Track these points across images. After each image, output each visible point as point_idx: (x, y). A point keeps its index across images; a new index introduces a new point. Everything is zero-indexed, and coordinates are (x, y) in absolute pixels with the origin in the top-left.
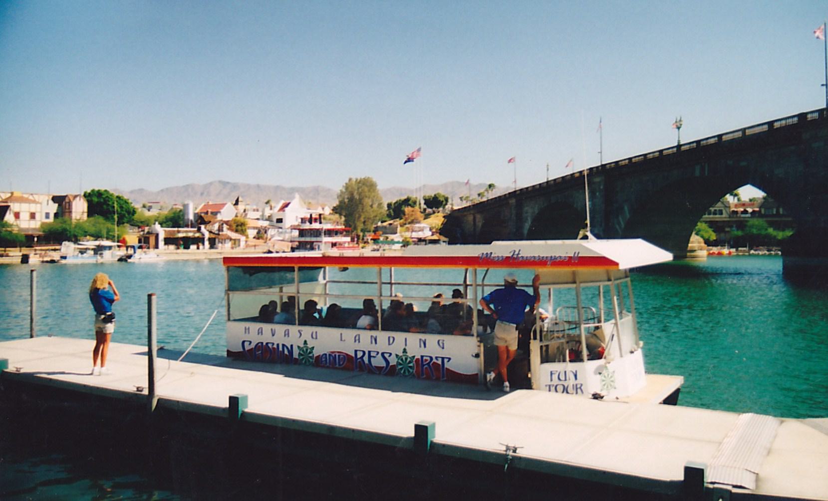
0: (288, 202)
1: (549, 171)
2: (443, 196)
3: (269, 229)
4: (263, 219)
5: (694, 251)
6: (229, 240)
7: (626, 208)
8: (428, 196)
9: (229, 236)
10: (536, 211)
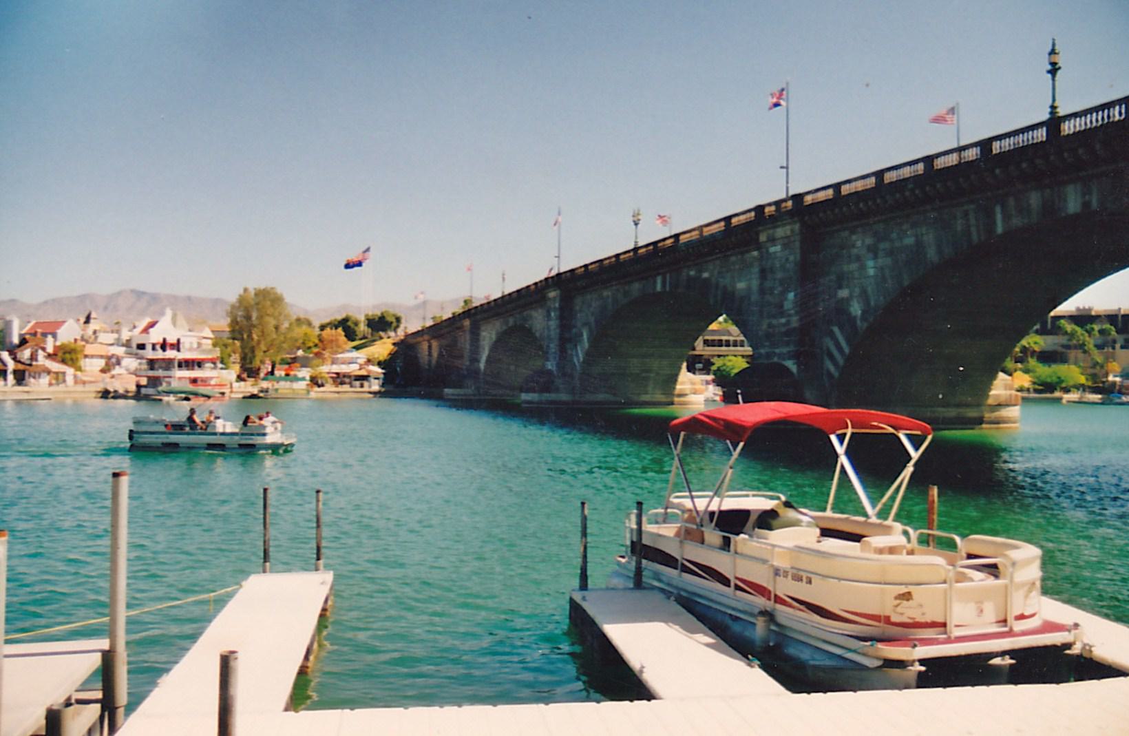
0: (155, 320)
1: (506, 281)
2: (394, 315)
3: (123, 357)
4: (118, 345)
5: (684, 395)
6: (46, 374)
7: (585, 336)
8: (373, 315)
9: (47, 368)
10: (494, 337)
